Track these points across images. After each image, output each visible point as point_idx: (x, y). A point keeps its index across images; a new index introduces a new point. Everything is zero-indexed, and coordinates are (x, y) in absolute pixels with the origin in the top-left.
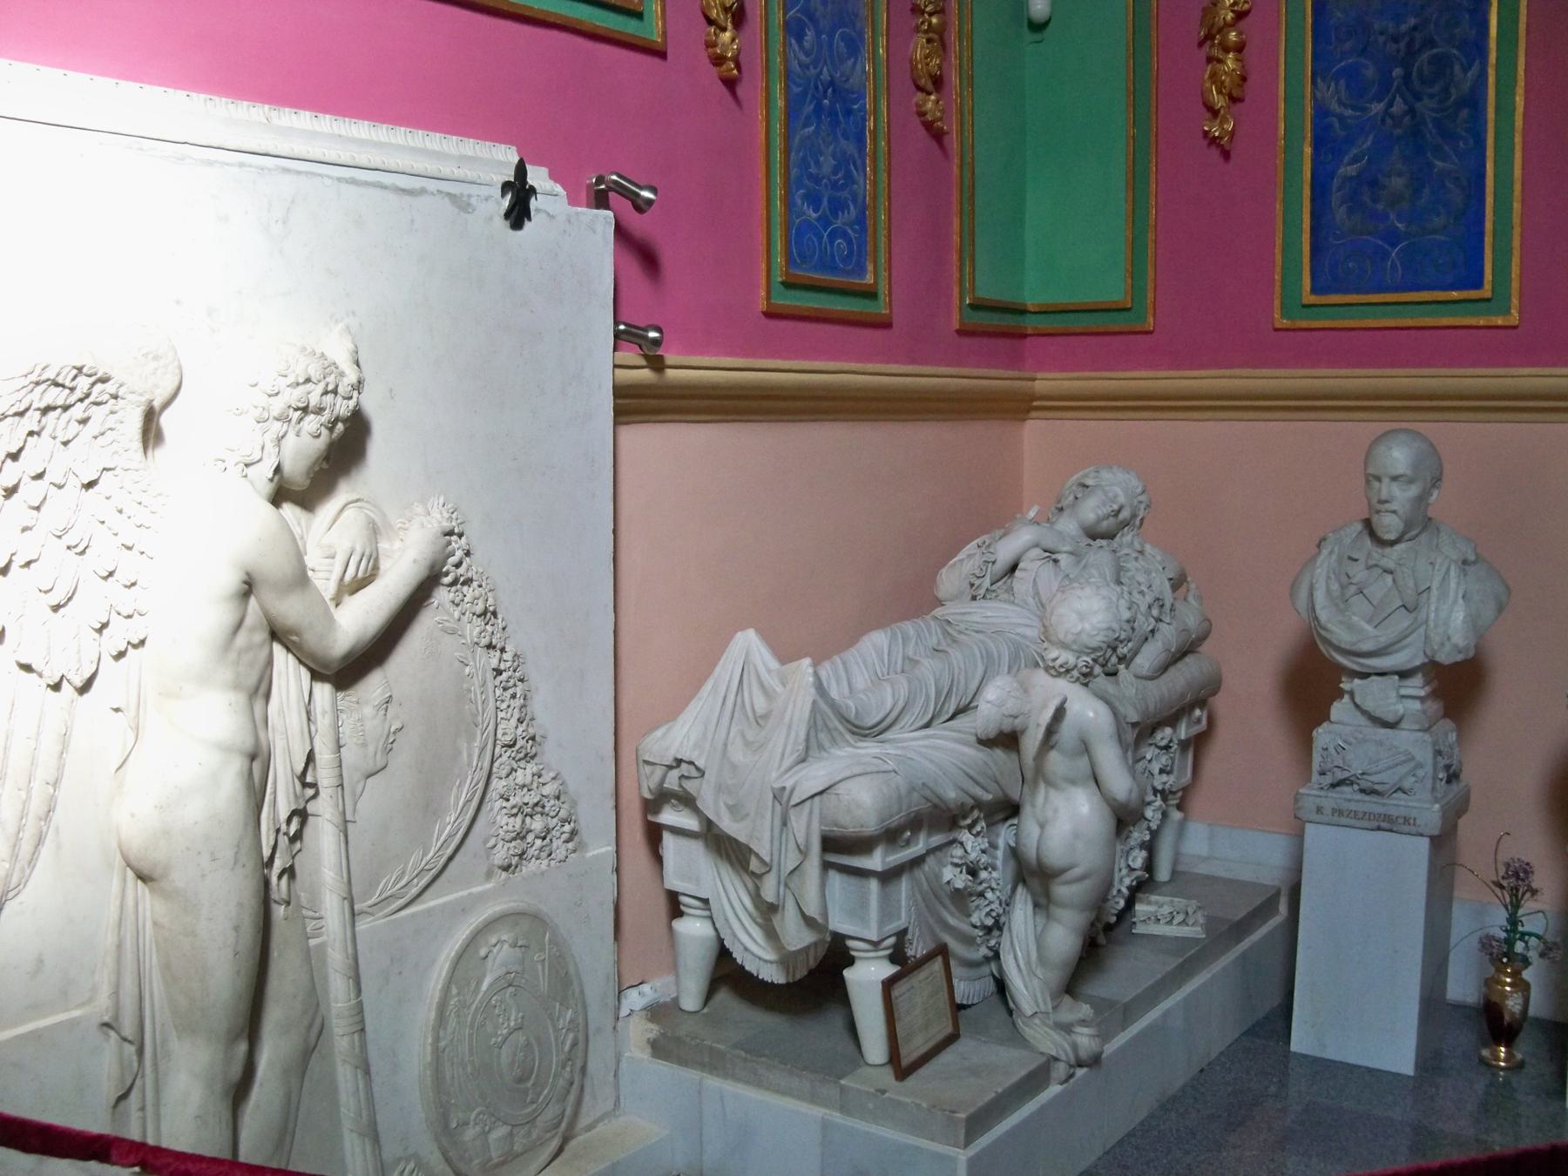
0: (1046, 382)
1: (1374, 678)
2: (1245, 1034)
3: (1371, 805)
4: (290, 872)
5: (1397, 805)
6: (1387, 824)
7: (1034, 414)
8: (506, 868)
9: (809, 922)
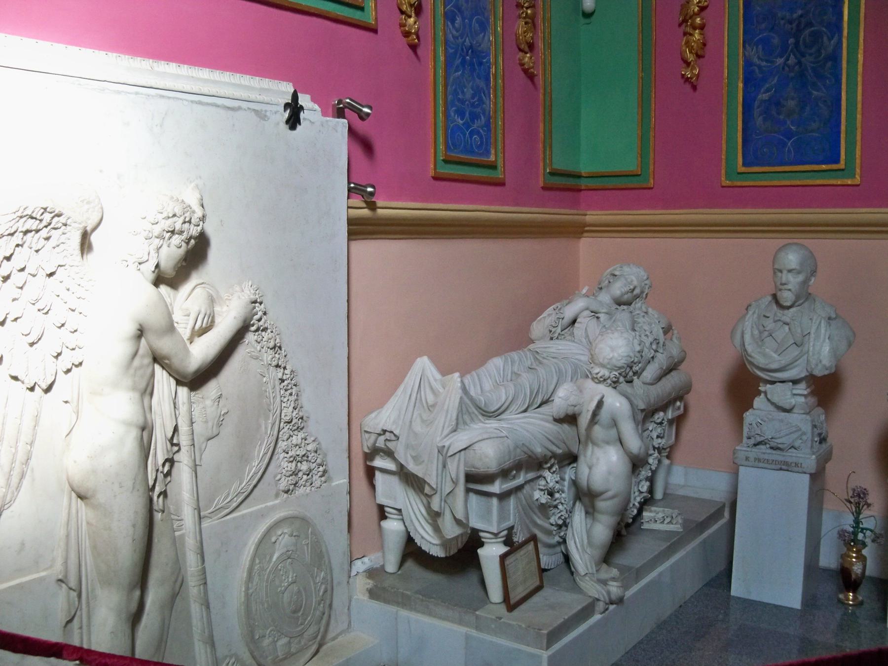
0: (593, 216)
1: (778, 384)
2: (706, 585)
3: (776, 456)
4: (164, 494)
5: (791, 456)
6: (785, 467)
7: (585, 234)
8: (287, 492)
9: (458, 522)
